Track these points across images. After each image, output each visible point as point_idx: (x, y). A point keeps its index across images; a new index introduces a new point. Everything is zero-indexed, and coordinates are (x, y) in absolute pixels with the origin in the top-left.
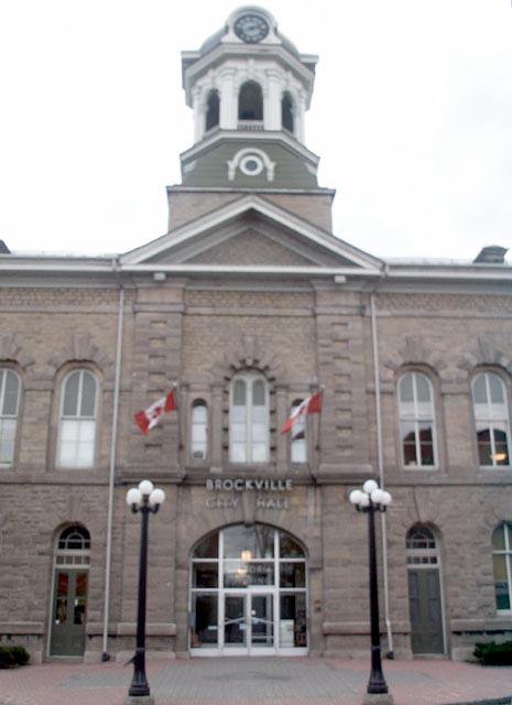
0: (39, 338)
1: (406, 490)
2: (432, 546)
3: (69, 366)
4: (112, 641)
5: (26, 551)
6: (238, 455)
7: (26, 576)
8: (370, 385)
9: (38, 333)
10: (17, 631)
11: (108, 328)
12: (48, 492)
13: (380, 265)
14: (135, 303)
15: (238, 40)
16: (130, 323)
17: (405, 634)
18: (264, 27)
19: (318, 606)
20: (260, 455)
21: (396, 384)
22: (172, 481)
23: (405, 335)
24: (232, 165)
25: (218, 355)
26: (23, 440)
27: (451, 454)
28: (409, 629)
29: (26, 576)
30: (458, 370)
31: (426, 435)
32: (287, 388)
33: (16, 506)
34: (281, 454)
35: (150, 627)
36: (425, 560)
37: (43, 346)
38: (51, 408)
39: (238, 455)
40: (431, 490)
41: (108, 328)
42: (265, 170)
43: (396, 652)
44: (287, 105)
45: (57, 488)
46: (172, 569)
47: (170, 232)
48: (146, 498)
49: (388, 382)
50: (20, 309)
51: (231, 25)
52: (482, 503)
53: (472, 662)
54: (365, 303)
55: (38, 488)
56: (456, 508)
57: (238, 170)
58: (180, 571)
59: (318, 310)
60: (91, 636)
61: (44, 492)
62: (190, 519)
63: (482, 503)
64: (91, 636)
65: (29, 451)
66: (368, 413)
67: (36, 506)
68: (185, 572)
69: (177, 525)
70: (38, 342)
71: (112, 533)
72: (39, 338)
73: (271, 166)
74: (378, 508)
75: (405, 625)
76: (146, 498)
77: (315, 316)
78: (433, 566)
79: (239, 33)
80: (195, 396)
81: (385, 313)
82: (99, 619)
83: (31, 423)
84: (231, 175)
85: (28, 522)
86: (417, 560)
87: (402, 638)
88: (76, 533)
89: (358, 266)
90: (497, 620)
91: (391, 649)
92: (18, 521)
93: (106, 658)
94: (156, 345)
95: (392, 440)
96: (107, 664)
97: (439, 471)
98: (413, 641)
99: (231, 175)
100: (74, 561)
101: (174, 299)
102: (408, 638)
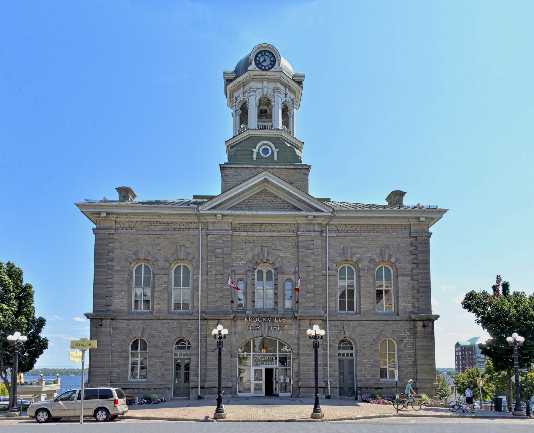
0: (159, 248)
1: (340, 322)
2: (352, 348)
3: (175, 262)
4: (203, 390)
5: (160, 351)
6: (259, 305)
7: (160, 362)
8: (324, 272)
9: (159, 245)
10: (158, 386)
11: (194, 243)
12: (169, 323)
13: (331, 210)
14: (207, 229)
15: (257, 69)
16: (205, 241)
17: (336, 388)
18: (272, 59)
19: (296, 374)
20: (270, 304)
21: (337, 271)
22: (228, 318)
23: (343, 246)
24: (255, 151)
25: (249, 257)
26: (155, 299)
27: (362, 306)
28: (338, 386)
29: (160, 362)
30: (368, 264)
31: (351, 292)
32: (283, 273)
33: (153, 330)
34: (280, 305)
35: (223, 384)
36: (347, 355)
37: (161, 252)
38: (168, 283)
39: (259, 305)
40: (351, 322)
41: (194, 243)
42: (273, 154)
43: (332, 395)
44: (285, 111)
45: (173, 321)
46: (229, 358)
47: (222, 193)
48: (220, 332)
49: (333, 270)
50: (148, 233)
51: (252, 57)
52: (376, 329)
53: (144, 403)
54: (323, 229)
55: (165, 322)
56: (363, 331)
57: (258, 153)
58: (232, 359)
59: (299, 233)
60: (192, 388)
61: (167, 323)
62: (237, 335)
63: (376, 329)
64: (192, 388)
65: (159, 304)
66: (322, 285)
67: (164, 330)
68: (235, 359)
69: (231, 338)
70: (160, 250)
71: (201, 342)
72: (159, 248)
73: (276, 151)
74: (319, 337)
75: (336, 384)
76: (220, 332)
77: (298, 236)
78: (351, 358)
79: (258, 64)
80: (238, 277)
81: (333, 235)
82: (196, 379)
83: (159, 291)
84: (255, 156)
85: (160, 337)
86: (343, 355)
87: (335, 389)
88: (183, 342)
89: (322, 211)
90: (380, 383)
91: (329, 394)
92: (156, 337)
93: (200, 398)
94: (219, 251)
95: (334, 298)
96: (328, 400)
97: (356, 314)
98: (340, 391)
99: (255, 156)
100: (183, 355)
101: (227, 228)
102: (338, 389)
